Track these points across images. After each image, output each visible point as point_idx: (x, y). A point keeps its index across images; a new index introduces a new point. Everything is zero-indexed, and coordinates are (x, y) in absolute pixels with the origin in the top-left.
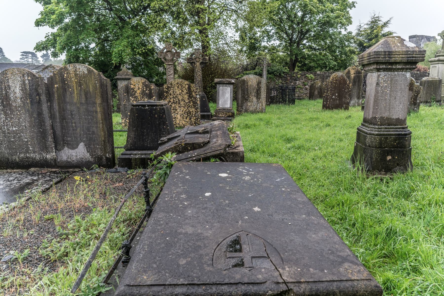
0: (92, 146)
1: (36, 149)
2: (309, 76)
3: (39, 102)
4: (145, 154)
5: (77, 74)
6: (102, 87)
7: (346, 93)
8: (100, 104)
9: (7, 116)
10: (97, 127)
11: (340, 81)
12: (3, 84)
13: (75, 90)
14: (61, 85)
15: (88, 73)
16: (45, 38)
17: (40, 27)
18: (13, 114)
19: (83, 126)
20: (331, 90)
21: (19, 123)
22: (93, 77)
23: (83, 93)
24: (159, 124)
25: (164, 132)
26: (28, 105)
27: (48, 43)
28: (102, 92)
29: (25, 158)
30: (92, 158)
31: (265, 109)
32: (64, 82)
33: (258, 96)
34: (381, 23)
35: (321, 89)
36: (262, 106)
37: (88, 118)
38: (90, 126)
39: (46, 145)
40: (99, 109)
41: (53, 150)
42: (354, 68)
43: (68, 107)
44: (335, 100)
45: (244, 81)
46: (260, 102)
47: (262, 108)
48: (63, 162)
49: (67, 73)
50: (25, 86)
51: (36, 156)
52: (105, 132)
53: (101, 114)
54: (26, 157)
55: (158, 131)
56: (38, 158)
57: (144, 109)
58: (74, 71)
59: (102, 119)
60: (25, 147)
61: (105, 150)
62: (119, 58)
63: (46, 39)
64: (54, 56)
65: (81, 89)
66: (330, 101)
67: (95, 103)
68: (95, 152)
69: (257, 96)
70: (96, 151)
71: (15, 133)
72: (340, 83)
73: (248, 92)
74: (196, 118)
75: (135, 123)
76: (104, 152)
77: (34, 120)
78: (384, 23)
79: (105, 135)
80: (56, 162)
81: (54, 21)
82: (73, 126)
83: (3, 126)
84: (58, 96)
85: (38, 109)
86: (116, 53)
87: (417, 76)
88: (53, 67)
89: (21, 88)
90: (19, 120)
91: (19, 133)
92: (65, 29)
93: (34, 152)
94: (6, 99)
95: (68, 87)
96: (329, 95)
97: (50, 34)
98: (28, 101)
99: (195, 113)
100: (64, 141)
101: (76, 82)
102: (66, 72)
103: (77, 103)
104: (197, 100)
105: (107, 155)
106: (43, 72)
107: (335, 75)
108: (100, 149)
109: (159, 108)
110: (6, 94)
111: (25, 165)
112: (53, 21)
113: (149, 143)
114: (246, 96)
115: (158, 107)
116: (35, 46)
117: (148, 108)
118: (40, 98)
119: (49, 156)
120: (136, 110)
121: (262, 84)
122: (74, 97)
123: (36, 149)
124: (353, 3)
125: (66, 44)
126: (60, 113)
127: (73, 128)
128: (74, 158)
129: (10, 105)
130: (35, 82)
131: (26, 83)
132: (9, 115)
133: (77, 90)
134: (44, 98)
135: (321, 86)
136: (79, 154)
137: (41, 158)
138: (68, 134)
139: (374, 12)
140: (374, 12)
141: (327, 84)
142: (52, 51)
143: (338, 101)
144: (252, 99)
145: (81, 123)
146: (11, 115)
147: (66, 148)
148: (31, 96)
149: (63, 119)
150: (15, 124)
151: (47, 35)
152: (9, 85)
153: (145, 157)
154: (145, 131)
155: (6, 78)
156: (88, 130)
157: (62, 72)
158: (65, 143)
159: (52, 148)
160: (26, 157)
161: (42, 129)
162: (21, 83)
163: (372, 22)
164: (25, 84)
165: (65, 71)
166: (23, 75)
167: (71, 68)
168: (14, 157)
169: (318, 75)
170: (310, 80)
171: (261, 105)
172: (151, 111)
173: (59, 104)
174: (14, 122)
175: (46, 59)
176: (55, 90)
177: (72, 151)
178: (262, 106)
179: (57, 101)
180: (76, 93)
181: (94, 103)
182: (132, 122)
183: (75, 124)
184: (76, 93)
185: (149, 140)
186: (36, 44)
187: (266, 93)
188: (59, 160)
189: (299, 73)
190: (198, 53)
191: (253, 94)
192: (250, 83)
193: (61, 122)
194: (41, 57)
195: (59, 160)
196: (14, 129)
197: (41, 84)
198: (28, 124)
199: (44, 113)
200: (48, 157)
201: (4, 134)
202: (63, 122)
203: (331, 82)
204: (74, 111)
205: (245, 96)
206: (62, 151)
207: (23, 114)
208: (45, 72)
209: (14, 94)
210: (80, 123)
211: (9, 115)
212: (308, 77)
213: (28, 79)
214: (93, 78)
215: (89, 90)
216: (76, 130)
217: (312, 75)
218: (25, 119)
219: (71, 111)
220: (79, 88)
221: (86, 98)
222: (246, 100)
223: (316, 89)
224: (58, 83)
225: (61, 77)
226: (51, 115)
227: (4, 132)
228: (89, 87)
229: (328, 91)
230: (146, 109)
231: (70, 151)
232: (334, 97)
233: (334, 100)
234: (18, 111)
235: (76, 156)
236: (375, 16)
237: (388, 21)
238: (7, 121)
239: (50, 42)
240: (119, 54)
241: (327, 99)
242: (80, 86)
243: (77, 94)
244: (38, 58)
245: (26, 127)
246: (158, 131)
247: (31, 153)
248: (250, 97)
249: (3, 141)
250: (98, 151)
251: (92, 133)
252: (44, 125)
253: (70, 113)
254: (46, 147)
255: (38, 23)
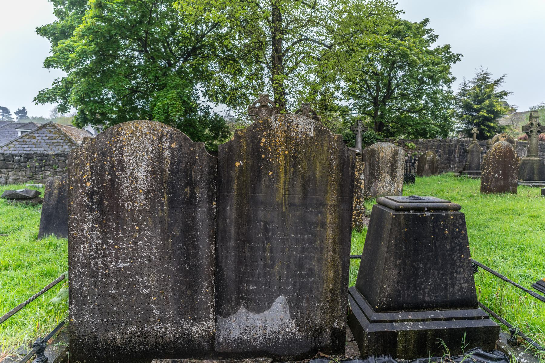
0: (304, 304)
1: (169, 314)
2: (409, 144)
3: (191, 202)
4: (423, 320)
5: (291, 139)
6: (343, 167)
7: (514, 170)
8: (334, 206)
9: (106, 234)
10: (320, 260)
11: (505, 154)
12: (108, 159)
13: (282, 175)
14: (249, 162)
15: (317, 135)
16: (53, 85)
17: (51, 69)
18: (123, 229)
19: (289, 257)
20: (493, 166)
21: (134, 250)
22: (326, 145)
23: (298, 181)
24: (452, 249)
25: (460, 267)
26: (163, 207)
27: (57, 93)
28: (342, 179)
29: (139, 336)
30: (300, 330)
31: (402, 192)
32: (260, 154)
33: (393, 173)
34: (491, 81)
35: (433, 162)
36: (398, 187)
37: (303, 240)
38: (306, 258)
39: (193, 303)
40: (329, 219)
41: (209, 313)
42: (504, 135)
43: (261, 214)
44: (498, 180)
45: (373, 151)
46: (395, 182)
47: (398, 191)
48: (229, 342)
49: (268, 136)
50: (160, 162)
51: (166, 329)
52: (338, 271)
53: (334, 229)
54: (142, 333)
55: (449, 266)
56: (171, 335)
57: (423, 217)
58: (285, 131)
59: (334, 242)
60: (143, 309)
61: (332, 312)
62: (163, 115)
63: (54, 86)
64: (62, 109)
65: (294, 172)
66: (491, 181)
67: (323, 204)
68: (309, 316)
69: (392, 173)
70: (312, 315)
71: (121, 276)
72: (505, 157)
73: (378, 168)
74: (357, 213)
75: (402, 248)
76: (328, 317)
77: (173, 243)
78: (495, 81)
79: (335, 278)
80: (213, 343)
81: (73, 61)
82: (265, 257)
83: (94, 258)
84: (240, 188)
85: (185, 217)
86: (159, 109)
87: (543, 147)
88: (54, 125)
89: (150, 168)
90: (135, 243)
91: (131, 276)
92: (84, 73)
93: (163, 320)
94: (111, 194)
95: (266, 168)
96: (490, 173)
97: (60, 80)
98: (164, 200)
99: (356, 205)
100: (239, 292)
101: (286, 156)
102: (265, 133)
103: (282, 204)
104: (360, 183)
105: (335, 323)
106: (38, 132)
107: (498, 146)
108: (322, 309)
109: (454, 215)
110: (112, 181)
111: (136, 353)
112: (72, 61)
113: (428, 293)
114: (376, 173)
115: (450, 213)
116: (36, 96)
117: (431, 216)
118: (193, 193)
119: (197, 330)
120: (405, 219)
121: (399, 156)
122: (277, 190)
123: (169, 314)
124: (458, 55)
125: (86, 94)
126: (238, 226)
127: (266, 261)
128: (259, 333)
129: (117, 208)
130: (186, 154)
131: (165, 156)
132: (112, 233)
133: (286, 174)
134: (202, 191)
135: (433, 159)
136: (271, 324)
137: (177, 336)
138: (253, 276)
139: (481, 67)
140: (481, 67)
141: (487, 157)
142: (59, 103)
143: (502, 182)
144: (384, 177)
145: (287, 250)
146: (117, 232)
147: (242, 310)
148: (173, 187)
149: (244, 242)
150: (125, 254)
151: (56, 81)
152: (120, 162)
153: (426, 328)
154: (421, 265)
155: (116, 143)
156: (300, 265)
157: (255, 133)
158: (242, 298)
159: (207, 309)
160: (142, 333)
161: (189, 265)
162: (152, 155)
163: (480, 79)
164: (162, 158)
165: (263, 131)
166: (160, 139)
167: (278, 123)
168: (111, 334)
169: (421, 143)
170: (411, 150)
171: (396, 186)
172: (437, 219)
173: (240, 205)
174: (123, 249)
175: (21, 116)
176: (234, 174)
177: (257, 316)
178: (398, 187)
179: (235, 200)
180: (282, 180)
181: (321, 204)
182: (396, 245)
183: (271, 251)
184: (282, 180)
185: (428, 287)
186: (38, 93)
187: (404, 168)
188: (221, 338)
189: (396, 141)
190: (306, 109)
191: (386, 170)
192: (382, 154)
193: (239, 249)
194: (15, 113)
195: (221, 338)
196: (121, 265)
197: (200, 160)
198: (155, 254)
199: (199, 226)
200: (194, 330)
201: (93, 277)
202: (243, 248)
203: (494, 155)
204: (272, 222)
205: (374, 172)
206: (233, 317)
207: (148, 230)
208: (42, 132)
209: (132, 182)
210: (283, 250)
211: (112, 233)
212: (408, 146)
213: (170, 147)
214: (325, 148)
215: (314, 175)
216: (272, 266)
217: (413, 144)
218: (150, 241)
219: (266, 223)
220: (292, 169)
221: (305, 193)
222: (376, 178)
223: (426, 162)
224: (245, 157)
225: (253, 143)
226: (216, 233)
227: (93, 272)
228: (316, 167)
229: (489, 167)
230: (427, 217)
231: (252, 315)
232: (496, 176)
233: (497, 179)
234: (136, 222)
235: (265, 328)
236: (483, 73)
237: (501, 79)
238: (105, 246)
239: (60, 90)
240: (164, 109)
241: (487, 178)
242: (294, 166)
243: (285, 182)
244: (11, 114)
245: (150, 261)
246: (449, 266)
247: (155, 322)
248: (381, 175)
249: (89, 294)
250: (316, 316)
251: (307, 274)
252: (196, 255)
253: (262, 227)
254: (192, 307)
255: (48, 64)
